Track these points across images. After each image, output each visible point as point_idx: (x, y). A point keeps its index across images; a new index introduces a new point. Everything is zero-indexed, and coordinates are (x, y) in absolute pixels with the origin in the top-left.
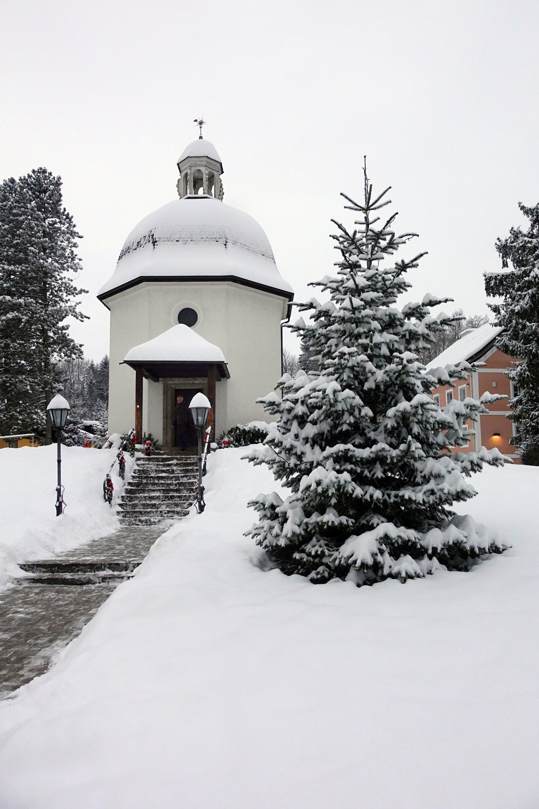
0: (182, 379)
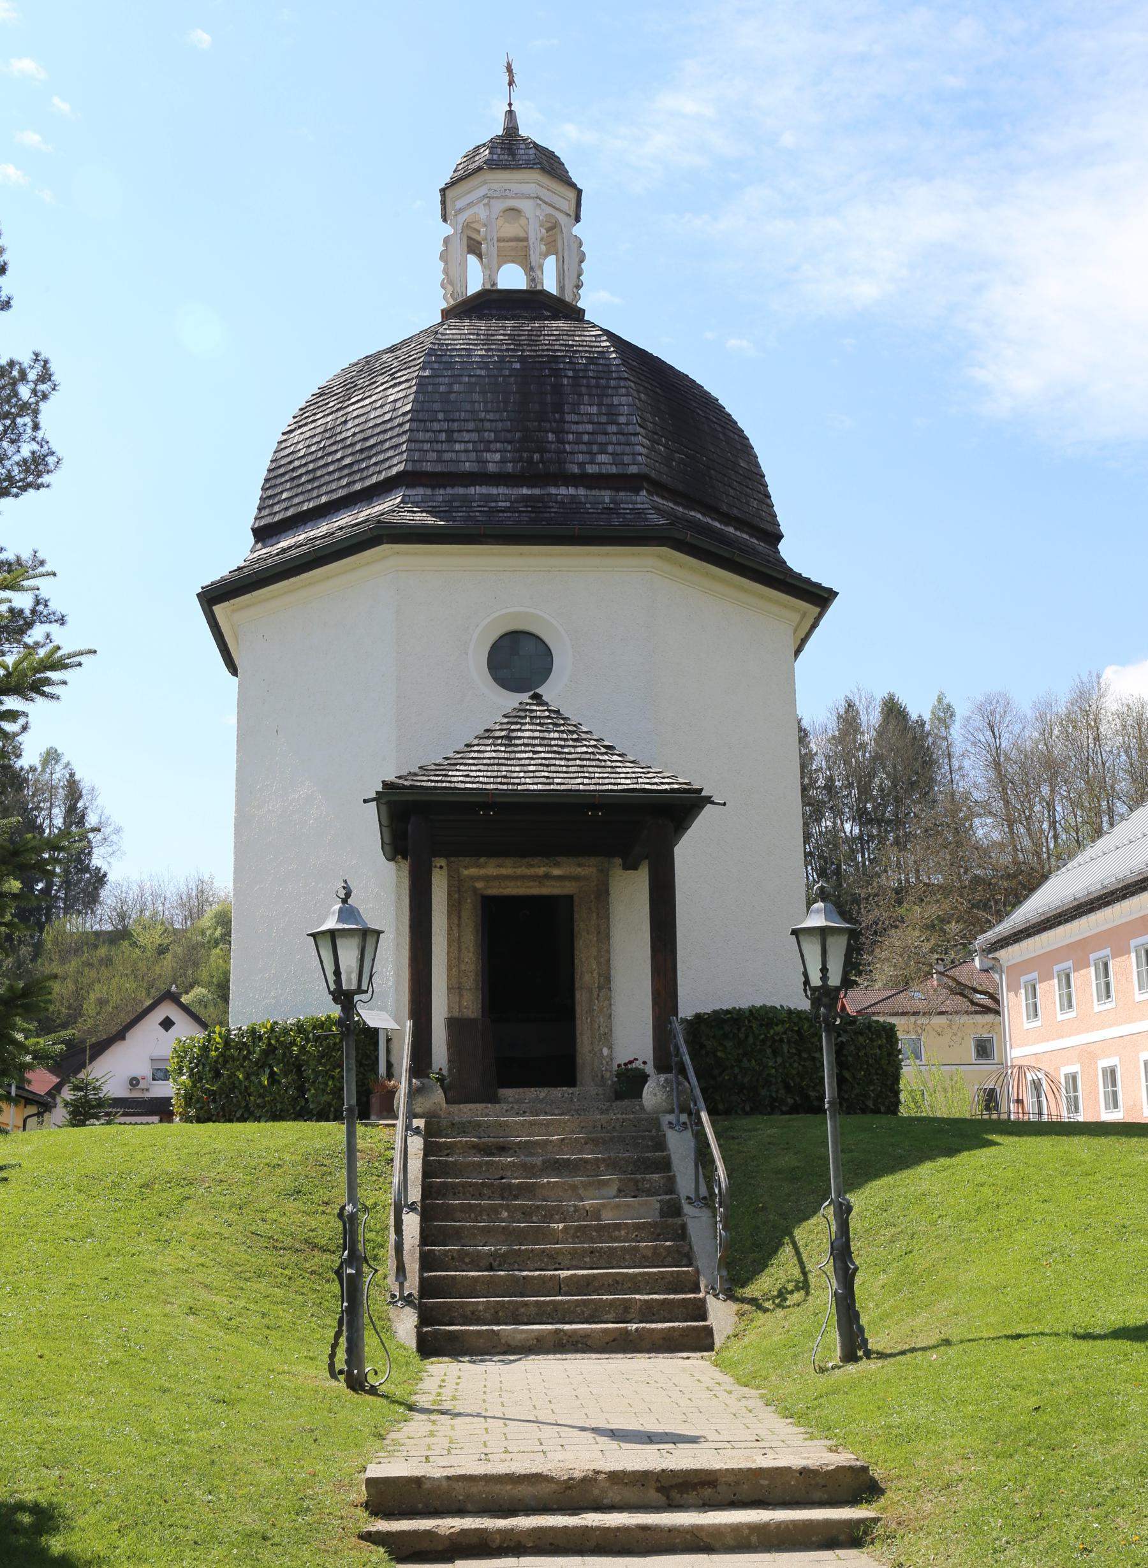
0: (509, 861)
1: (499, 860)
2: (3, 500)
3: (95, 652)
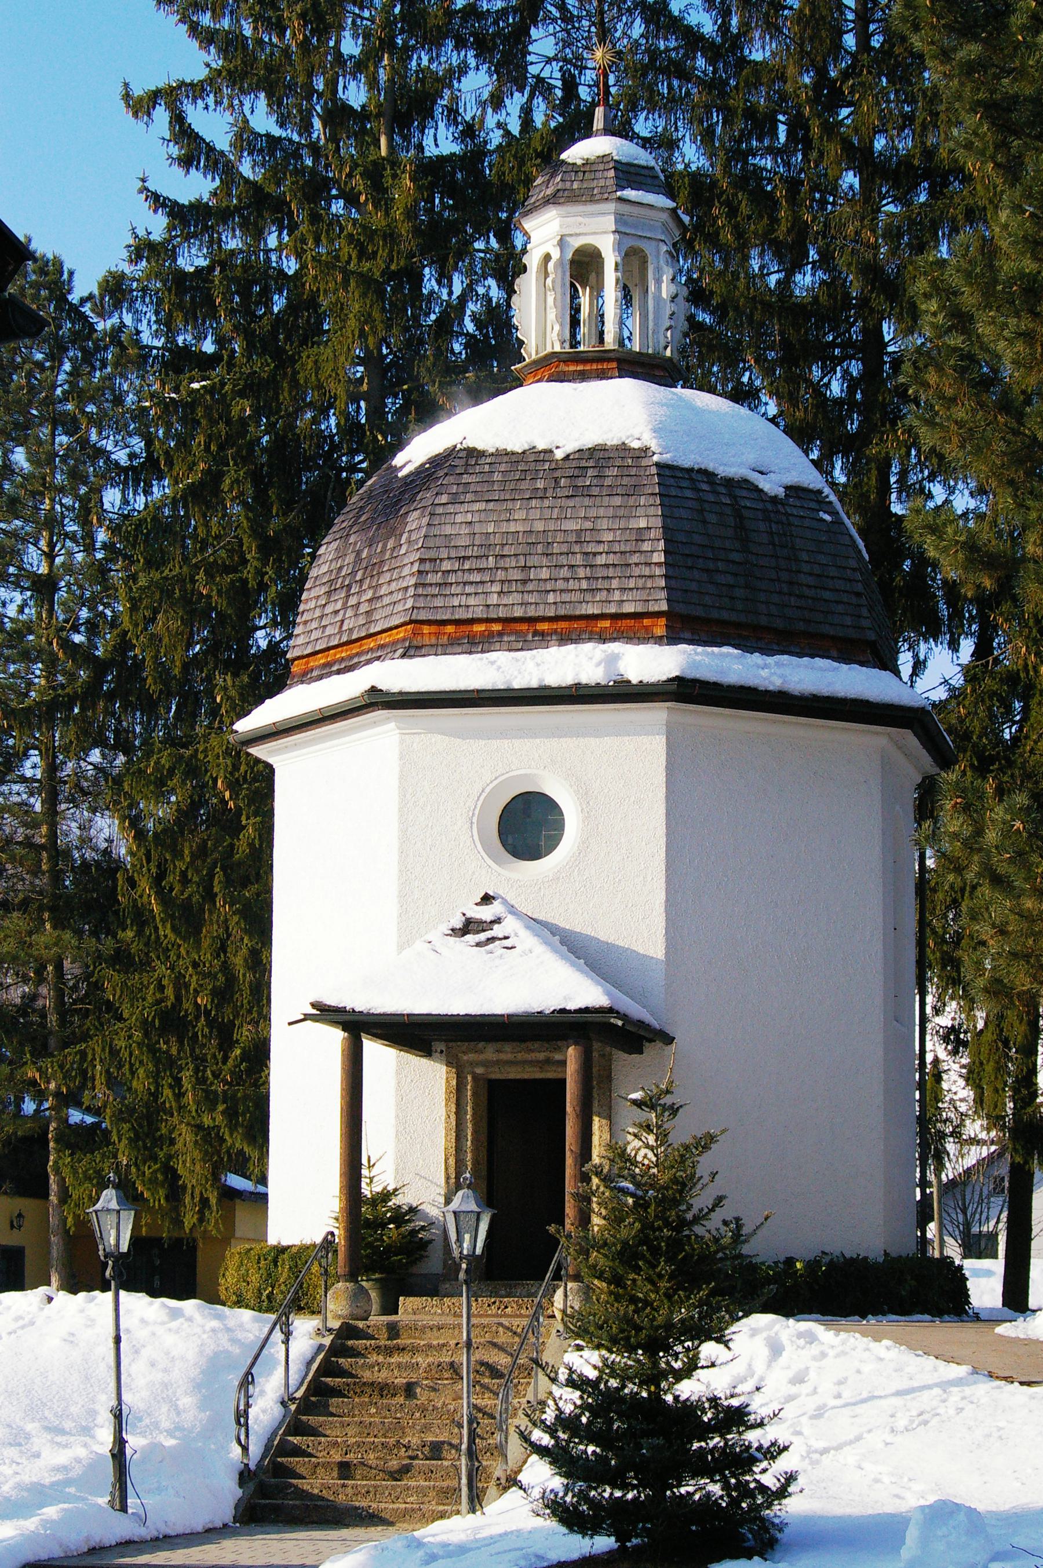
0: (508, 1047)
1: (498, 1045)
2: (12, 1298)
3: (290, 1024)
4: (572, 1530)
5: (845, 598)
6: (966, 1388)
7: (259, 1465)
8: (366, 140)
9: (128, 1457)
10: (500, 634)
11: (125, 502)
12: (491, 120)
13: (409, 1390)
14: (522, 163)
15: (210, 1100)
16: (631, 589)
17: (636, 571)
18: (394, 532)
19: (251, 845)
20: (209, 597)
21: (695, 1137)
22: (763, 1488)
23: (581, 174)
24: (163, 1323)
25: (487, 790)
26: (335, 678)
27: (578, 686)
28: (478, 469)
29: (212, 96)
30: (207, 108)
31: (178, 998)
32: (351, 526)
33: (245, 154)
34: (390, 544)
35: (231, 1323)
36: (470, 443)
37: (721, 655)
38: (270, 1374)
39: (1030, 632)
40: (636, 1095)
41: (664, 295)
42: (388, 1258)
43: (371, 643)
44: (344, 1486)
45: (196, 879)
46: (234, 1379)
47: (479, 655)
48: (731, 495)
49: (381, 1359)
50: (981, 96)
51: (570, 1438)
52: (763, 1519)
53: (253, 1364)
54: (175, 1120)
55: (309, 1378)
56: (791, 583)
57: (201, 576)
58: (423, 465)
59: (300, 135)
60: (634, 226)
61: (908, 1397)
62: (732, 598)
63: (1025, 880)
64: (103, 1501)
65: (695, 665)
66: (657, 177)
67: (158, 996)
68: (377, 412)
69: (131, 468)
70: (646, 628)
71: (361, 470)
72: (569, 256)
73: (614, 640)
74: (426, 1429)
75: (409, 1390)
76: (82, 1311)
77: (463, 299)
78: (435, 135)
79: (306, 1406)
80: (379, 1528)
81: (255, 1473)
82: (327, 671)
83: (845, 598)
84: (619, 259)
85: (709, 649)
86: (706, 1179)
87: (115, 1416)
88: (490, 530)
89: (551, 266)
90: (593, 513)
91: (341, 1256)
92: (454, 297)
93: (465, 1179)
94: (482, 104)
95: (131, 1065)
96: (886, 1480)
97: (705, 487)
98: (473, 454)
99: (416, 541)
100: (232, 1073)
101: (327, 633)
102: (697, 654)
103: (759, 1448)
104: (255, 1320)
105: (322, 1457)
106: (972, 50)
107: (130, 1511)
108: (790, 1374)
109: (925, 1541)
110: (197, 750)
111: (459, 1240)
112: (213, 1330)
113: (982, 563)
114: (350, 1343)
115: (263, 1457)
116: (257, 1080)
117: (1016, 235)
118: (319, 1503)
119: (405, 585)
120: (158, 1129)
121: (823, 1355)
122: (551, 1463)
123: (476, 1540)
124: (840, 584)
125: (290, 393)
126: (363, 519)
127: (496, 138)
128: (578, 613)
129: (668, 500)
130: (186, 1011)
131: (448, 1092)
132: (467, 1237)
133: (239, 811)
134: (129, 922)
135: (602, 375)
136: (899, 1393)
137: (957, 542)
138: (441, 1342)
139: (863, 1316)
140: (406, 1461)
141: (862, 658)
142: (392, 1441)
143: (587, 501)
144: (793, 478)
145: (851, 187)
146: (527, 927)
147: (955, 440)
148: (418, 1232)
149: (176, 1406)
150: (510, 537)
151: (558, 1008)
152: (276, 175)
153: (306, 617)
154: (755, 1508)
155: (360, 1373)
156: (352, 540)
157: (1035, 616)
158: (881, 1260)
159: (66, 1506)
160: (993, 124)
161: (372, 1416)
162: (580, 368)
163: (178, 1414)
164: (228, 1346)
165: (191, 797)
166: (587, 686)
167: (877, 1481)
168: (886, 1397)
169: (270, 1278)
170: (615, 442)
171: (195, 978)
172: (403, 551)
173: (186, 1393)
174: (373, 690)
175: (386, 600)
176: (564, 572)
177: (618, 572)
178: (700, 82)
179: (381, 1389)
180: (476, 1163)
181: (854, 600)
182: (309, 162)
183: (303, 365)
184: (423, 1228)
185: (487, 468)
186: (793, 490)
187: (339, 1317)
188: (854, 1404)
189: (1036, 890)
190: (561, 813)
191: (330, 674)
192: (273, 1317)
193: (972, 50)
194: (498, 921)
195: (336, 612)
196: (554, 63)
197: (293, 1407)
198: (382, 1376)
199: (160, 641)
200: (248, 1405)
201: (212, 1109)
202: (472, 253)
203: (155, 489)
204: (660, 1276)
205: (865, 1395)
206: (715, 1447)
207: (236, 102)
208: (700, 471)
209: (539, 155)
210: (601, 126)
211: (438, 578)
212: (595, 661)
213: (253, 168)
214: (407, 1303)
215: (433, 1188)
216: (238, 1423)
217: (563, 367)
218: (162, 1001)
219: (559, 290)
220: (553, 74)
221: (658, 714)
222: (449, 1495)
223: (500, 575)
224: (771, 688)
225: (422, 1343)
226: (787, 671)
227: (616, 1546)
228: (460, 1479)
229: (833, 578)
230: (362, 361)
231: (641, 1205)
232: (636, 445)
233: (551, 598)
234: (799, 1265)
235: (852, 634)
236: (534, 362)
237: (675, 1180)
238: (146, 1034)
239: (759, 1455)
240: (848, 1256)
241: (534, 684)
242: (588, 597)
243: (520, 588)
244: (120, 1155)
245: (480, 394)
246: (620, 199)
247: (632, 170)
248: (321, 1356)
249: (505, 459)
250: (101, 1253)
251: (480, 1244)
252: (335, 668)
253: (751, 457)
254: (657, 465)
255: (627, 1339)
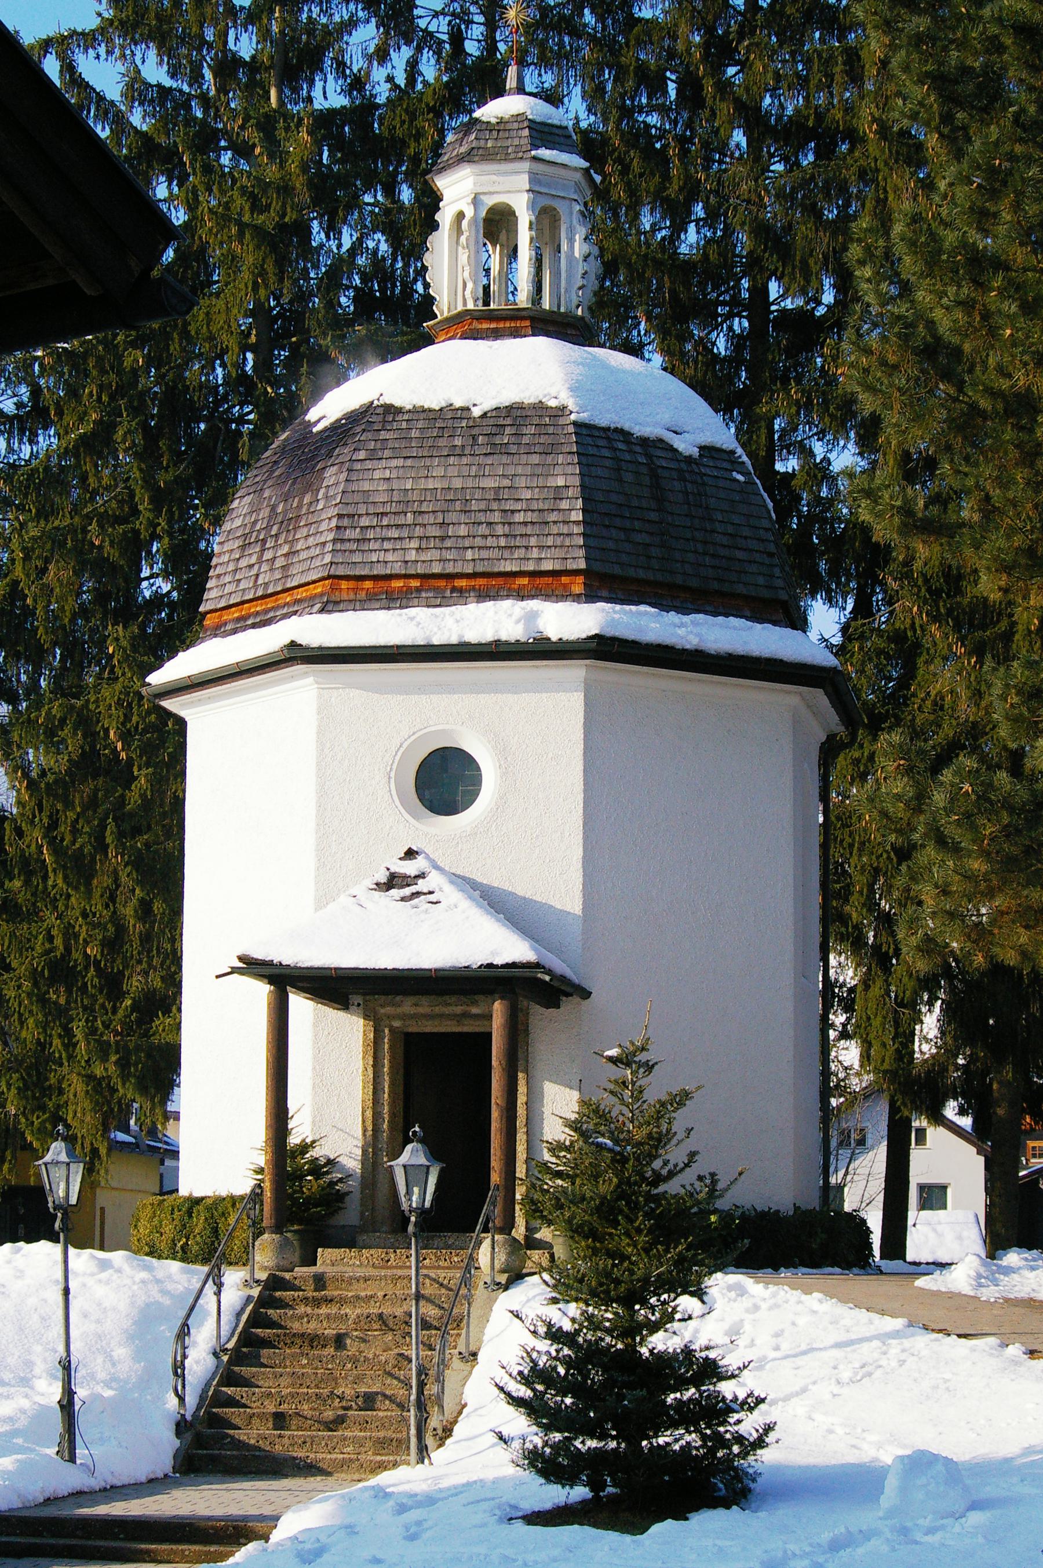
0: (424, 1000)
3: (218, 977)
4: (549, 1481)
5: (757, 557)
6: (904, 1340)
7: (195, 1415)
8: (255, 89)
9: (77, 1408)
10: (418, 590)
11: (10, 450)
12: (379, 74)
13: (339, 1341)
14: (413, 117)
15: (103, 1051)
16: (549, 547)
17: (555, 529)
18: (311, 487)
19: (143, 796)
20: (100, 547)
21: (669, 1094)
22: (739, 1439)
23: (495, 133)
24: (92, 1275)
25: (405, 746)
26: (251, 631)
27: (497, 643)
28: (395, 425)
29: (103, 45)
30: (98, 57)
31: (68, 949)
32: (265, 481)
33: (136, 104)
34: (307, 499)
35: (160, 1275)
36: (387, 400)
37: (639, 613)
38: (201, 1324)
39: (919, 591)
40: (613, 1052)
41: (577, 254)
42: (308, 1209)
43: (288, 598)
44: (280, 1436)
45: (86, 829)
46: (169, 1331)
47: (398, 611)
48: (647, 455)
49: (309, 1310)
50: (929, 68)
51: (546, 1390)
52: (736, 1469)
53: (188, 1316)
54: (65, 1069)
55: (239, 1329)
56: (705, 543)
57: (93, 527)
58: (339, 420)
59: (190, 86)
60: (548, 185)
61: (848, 1349)
62: (649, 557)
63: (974, 841)
64: (52, 1451)
65: (612, 622)
66: (570, 136)
67: (47, 946)
68: (264, 365)
69: (16, 416)
70: (565, 586)
71: (249, 422)
72: (483, 214)
73: (532, 597)
74: (358, 1380)
75: (339, 1341)
76: (9, 1262)
77: (353, 251)
78: (324, 88)
79: (238, 1357)
80: (319, 1478)
81: (192, 1424)
82: (242, 625)
83: (757, 557)
84: (533, 218)
85: (627, 608)
86: (680, 1135)
87: (64, 1368)
88: (408, 487)
89: (465, 224)
90: (511, 470)
91: (267, 1208)
92: (344, 249)
93: (415, 1132)
94: (370, 58)
95: (20, 1015)
96: (840, 1431)
97: (621, 446)
98: (390, 410)
99: (334, 497)
100: (123, 1023)
101: (242, 587)
102: (615, 612)
103: (735, 1399)
104: (184, 1271)
105: (256, 1408)
106: (921, 23)
107: (78, 1462)
108: (726, 1326)
109: (904, 1490)
110: (88, 701)
111: (409, 1193)
112: (143, 1282)
113: (916, 527)
114: (278, 1294)
115: (199, 1408)
116: (148, 1030)
117: (962, 206)
118: (257, 1453)
119: (323, 540)
120: (47, 1079)
121: (756, 1308)
122: (529, 1415)
123: (441, 1490)
124: (753, 544)
125: (180, 345)
126: (276, 474)
127: (382, 93)
128: (496, 570)
129: (586, 460)
130: (76, 960)
131: (365, 1045)
132: (416, 1190)
133: (130, 762)
134: (16, 871)
135: (516, 334)
136: (838, 1345)
137: (893, 507)
138: (369, 1293)
139: (776, 1269)
140: (341, 1412)
141: (774, 618)
142: (326, 1392)
143: (505, 459)
144: (708, 438)
145: (738, 146)
146: (452, 882)
147: (897, 406)
148: (336, 1183)
149: (111, 1356)
150: (428, 493)
151: (485, 962)
152: (165, 122)
153: (219, 570)
154: (729, 1459)
155: (289, 1324)
156: (266, 494)
157: (924, 575)
158: (791, 1213)
159: (19, 1457)
160: (941, 96)
161: (303, 1367)
162: (493, 325)
163: (114, 1365)
164: (158, 1297)
165: (82, 747)
166: (507, 643)
167: (830, 1431)
168: (825, 1349)
169: (185, 1230)
170: (532, 400)
171: (84, 928)
172: (320, 506)
173: (120, 1345)
174: (293, 644)
175: (303, 555)
176: (483, 530)
177: (537, 529)
178: (593, 39)
179: (312, 1341)
180: (393, 1115)
181: (767, 561)
182: (199, 114)
183: (194, 315)
184: (341, 1180)
185: (404, 425)
186: (707, 450)
187: (265, 1268)
188: (795, 1356)
189: (983, 851)
190: (478, 769)
191: (245, 628)
192: (206, 1269)
193: (921, 23)
194: (422, 876)
195: (251, 566)
196: (441, 18)
197: (225, 1358)
198: (312, 1327)
199: (52, 590)
200: (185, 1356)
201: (105, 1059)
202: (360, 206)
203: (41, 439)
204: (639, 1231)
205: (804, 1347)
206: (690, 1400)
207: (128, 52)
208: (616, 430)
209: (431, 110)
210: (514, 85)
211: (356, 534)
212: (514, 618)
213: (144, 117)
214: (324, 1255)
215: (350, 1140)
216: (176, 1374)
217: (476, 325)
218: (51, 951)
219: (472, 248)
220: (441, 27)
221: (576, 671)
222: (402, 1445)
223: (418, 531)
224: (688, 647)
225: (350, 1294)
226: (704, 631)
227: (590, 1495)
228: (409, 1429)
229: (746, 538)
230: (252, 313)
231: (618, 1161)
232: (553, 403)
233: (469, 554)
234: (713, 1218)
235: (766, 594)
236: (447, 320)
237: (650, 1136)
238: (36, 984)
239: (735, 1406)
240: (759, 1209)
241: (454, 640)
242: (507, 554)
243: (439, 544)
244: (9, 1105)
245: (389, 353)
246: (535, 159)
247: (546, 129)
248: (250, 1308)
249: (422, 416)
250: (50, 1205)
251: (429, 1197)
252: (249, 622)
253: (666, 417)
254: (575, 424)
255: (607, 1292)
